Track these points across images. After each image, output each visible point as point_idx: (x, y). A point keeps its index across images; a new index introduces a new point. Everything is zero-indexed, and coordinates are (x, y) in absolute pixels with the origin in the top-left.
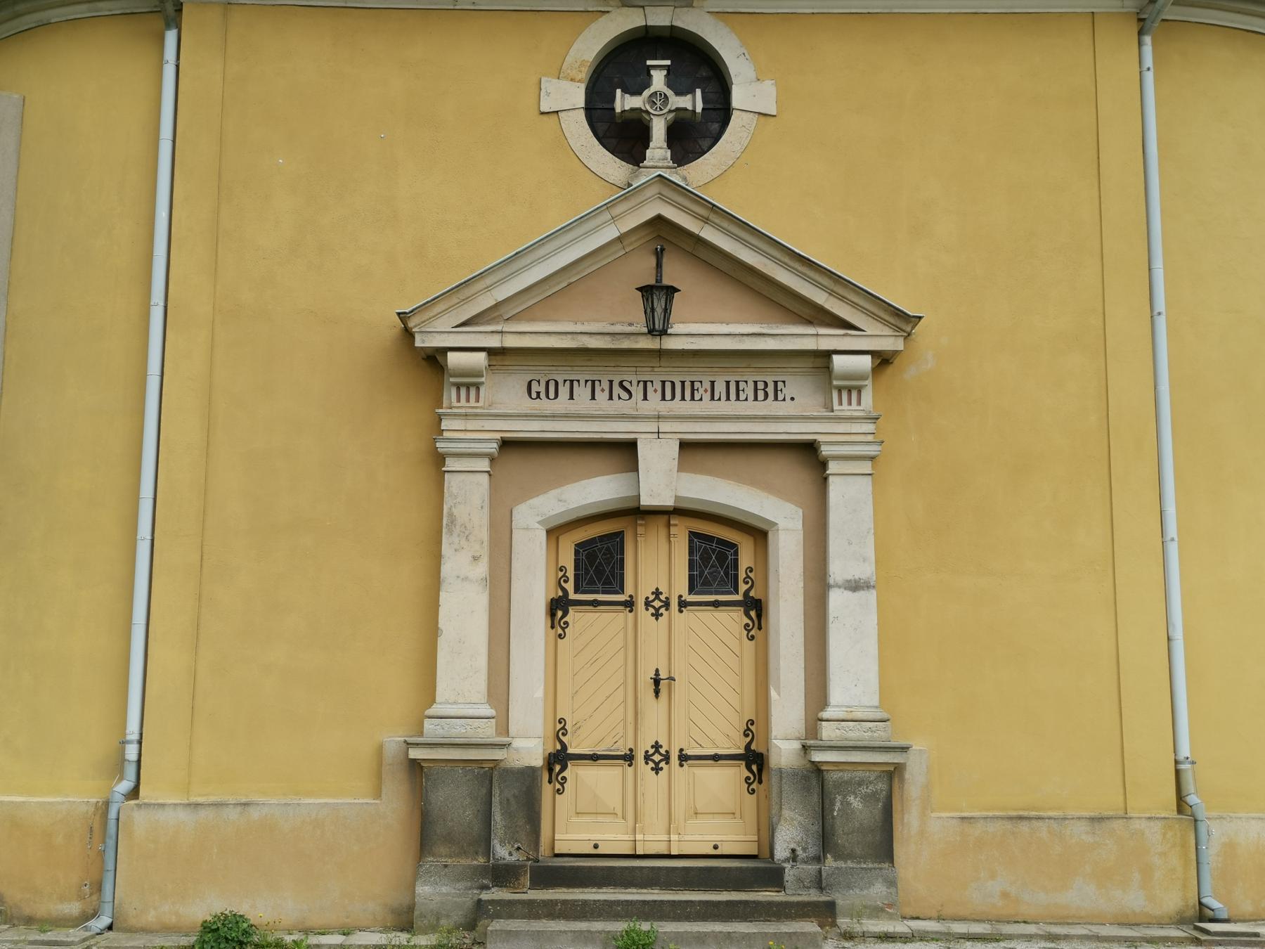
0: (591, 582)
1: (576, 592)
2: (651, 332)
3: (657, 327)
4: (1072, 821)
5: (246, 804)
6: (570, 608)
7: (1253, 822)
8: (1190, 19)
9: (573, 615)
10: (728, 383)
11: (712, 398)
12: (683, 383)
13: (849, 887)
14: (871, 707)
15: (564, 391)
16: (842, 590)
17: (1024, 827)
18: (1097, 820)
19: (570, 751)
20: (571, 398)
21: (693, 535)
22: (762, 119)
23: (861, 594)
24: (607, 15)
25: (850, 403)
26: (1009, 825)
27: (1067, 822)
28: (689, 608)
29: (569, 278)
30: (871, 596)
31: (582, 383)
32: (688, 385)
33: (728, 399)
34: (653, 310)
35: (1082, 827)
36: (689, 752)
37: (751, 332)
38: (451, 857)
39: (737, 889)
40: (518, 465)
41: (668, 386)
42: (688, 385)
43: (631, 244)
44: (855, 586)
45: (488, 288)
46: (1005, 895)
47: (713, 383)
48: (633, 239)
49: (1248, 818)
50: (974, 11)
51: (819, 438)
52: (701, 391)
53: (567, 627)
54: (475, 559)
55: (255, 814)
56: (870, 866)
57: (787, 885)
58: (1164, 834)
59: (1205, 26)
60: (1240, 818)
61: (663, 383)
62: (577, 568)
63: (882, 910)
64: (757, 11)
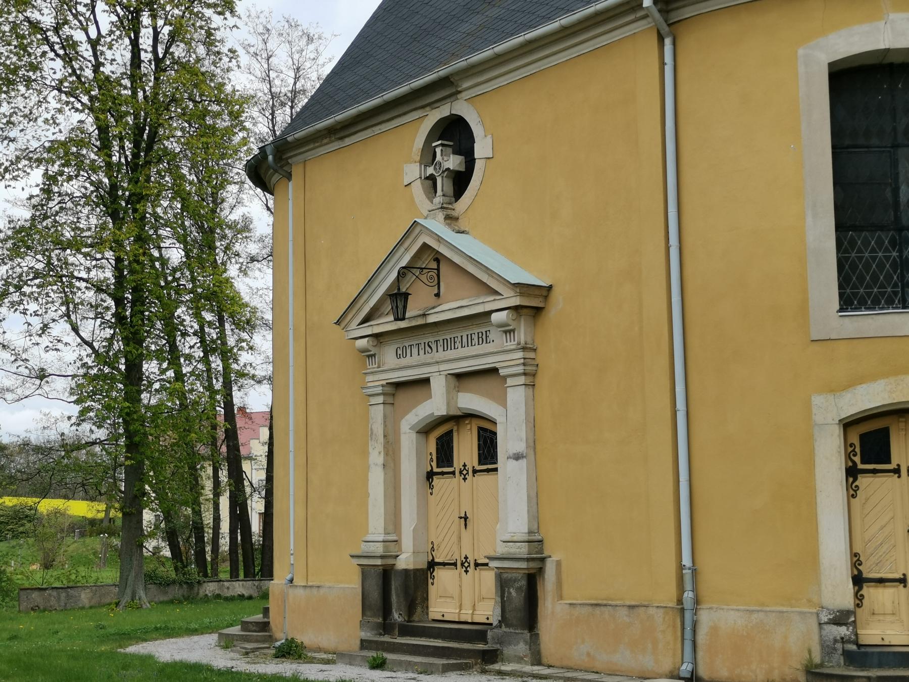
0: (443, 461)
1: (438, 467)
2: (397, 319)
3: (400, 317)
4: (620, 608)
5: (318, 587)
6: (434, 477)
7: (732, 613)
8: (702, 12)
9: (436, 481)
10: (467, 335)
11: (462, 347)
12: (451, 338)
13: (510, 644)
14: (523, 533)
15: (415, 351)
16: (512, 460)
17: (598, 611)
18: (631, 607)
19: (437, 560)
20: (411, 356)
21: (480, 429)
22: (488, 161)
23: (520, 461)
24: (427, 118)
25: (511, 341)
26: (590, 609)
27: (617, 608)
28: (478, 474)
29: (406, 285)
30: (523, 462)
31: (433, 342)
32: (452, 339)
33: (468, 346)
34: (397, 307)
35: (624, 612)
36: (479, 562)
37: (457, 306)
38: (371, 617)
39: (469, 642)
40: (403, 397)
41: (445, 340)
42: (452, 339)
43: (426, 260)
44: (517, 457)
45: (367, 301)
46: (588, 654)
47: (462, 336)
48: (426, 256)
49: (728, 609)
50: (577, 54)
51: (497, 365)
52: (458, 342)
53: (858, 490)
54: (380, 453)
55: (322, 591)
56: (520, 631)
57: (489, 641)
58: (664, 618)
59: (733, 7)
60: (723, 609)
61: (443, 340)
62: (437, 453)
63: (522, 658)
64: (485, 91)
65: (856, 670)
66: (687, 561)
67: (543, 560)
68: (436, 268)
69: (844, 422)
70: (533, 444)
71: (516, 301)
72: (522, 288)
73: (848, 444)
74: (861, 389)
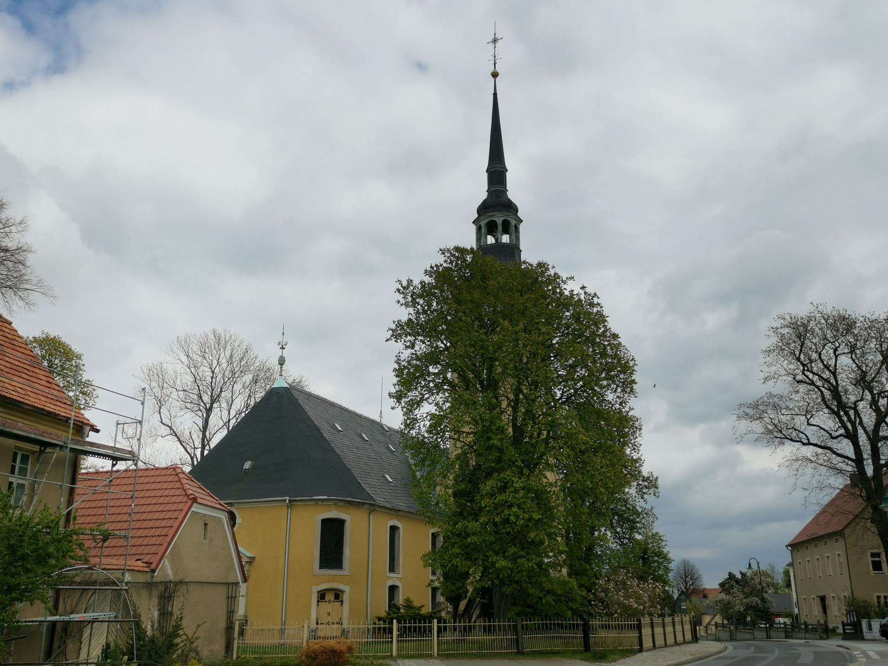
30: (244, 597)
44: (243, 596)
65: (399, 596)
66: (283, 620)
67: (247, 620)
68: (686, 641)
69: (871, 569)
70: (247, 593)
71: (248, 560)
72: (250, 558)
73: (318, 596)
74: (322, 585)
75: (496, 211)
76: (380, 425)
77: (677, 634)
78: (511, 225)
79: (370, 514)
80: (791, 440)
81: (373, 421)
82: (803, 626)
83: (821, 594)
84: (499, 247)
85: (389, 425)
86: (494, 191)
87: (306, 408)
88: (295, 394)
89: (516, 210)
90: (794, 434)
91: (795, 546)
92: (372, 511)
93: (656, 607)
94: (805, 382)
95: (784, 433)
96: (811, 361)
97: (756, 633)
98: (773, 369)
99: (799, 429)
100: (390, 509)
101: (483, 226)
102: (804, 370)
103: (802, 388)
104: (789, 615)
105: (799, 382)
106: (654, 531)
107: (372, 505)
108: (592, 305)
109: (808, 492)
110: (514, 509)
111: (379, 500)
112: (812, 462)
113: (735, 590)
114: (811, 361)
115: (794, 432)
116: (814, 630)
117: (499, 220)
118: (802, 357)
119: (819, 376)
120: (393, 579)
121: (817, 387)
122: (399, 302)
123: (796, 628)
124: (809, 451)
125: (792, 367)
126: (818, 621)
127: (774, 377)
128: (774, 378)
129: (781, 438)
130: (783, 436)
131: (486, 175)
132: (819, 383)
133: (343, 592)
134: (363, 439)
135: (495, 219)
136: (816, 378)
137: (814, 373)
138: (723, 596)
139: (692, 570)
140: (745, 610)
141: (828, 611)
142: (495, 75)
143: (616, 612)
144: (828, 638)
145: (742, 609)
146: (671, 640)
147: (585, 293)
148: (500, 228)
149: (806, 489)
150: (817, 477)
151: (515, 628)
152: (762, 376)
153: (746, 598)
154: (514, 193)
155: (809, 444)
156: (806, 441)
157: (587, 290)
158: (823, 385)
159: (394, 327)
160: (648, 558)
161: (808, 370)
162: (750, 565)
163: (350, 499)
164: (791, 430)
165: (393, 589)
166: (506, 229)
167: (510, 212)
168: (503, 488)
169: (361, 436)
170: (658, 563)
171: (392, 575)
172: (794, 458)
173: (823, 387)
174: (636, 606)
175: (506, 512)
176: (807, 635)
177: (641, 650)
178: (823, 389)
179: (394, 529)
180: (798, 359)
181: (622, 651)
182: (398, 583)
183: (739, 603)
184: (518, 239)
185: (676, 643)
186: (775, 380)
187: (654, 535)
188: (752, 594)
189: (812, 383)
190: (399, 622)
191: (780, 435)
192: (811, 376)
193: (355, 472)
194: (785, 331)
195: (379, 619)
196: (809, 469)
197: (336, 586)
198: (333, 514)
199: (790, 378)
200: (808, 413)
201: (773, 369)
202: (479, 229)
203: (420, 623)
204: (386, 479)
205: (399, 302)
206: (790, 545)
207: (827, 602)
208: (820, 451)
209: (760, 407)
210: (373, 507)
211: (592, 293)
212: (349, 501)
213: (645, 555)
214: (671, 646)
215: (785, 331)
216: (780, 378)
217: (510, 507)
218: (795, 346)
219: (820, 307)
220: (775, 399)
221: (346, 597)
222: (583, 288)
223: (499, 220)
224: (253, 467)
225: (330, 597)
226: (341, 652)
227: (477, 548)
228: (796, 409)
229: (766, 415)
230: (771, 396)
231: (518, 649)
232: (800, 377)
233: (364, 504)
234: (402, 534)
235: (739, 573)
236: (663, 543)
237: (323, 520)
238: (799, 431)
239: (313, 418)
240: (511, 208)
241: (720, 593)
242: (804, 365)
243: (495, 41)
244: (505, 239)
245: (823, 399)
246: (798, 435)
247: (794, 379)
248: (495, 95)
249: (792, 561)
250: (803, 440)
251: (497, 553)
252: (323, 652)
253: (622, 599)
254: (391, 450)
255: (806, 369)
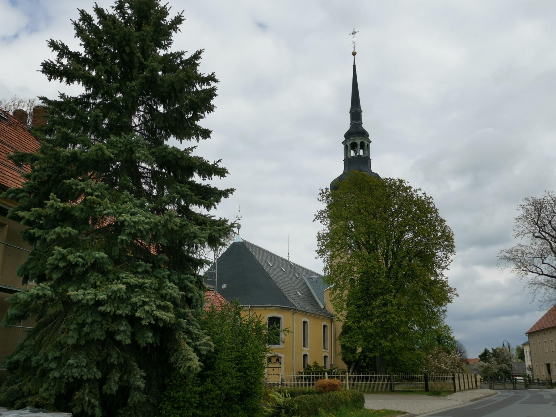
75: (356, 136)
76: (287, 262)
77: (461, 384)
78: (365, 146)
79: (293, 315)
80: (532, 272)
81: (285, 260)
82: (536, 381)
83: (547, 362)
84: (358, 158)
85: (293, 262)
86: (354, 124)
87: (253, 253)
88: (247, 245)
89: (368, 136)
90: (534, 268)
91: (530, 334)
92: (295, 313)
93: (456, 369)
94: (542, 238)
95: (528, 268)
96: (544, 225)
97: (507, 385)
98: (521, 229)
99: (537, 265)
100: (303, 312)
101: (348, 145)
102: (540, 230)
103: (540, 242)
104: (524, 376)
105: (537, 237)
106: (445, 324)
107: (294, 309)
108: (429, 203)
109: (542, 303)
110: (393, 315)
111: (298, 306)
112: (544, 285)
113: (492, 360)
114: (544, 225)
115: (534, 267)
116: (544, 383)
117: (358, 142)
118: (539, 223)
119: (549, 234)
120: (305, 351)
121: (548, 240)
122: (318, 199)
123: (529, 383)
124: (542, 278)
125: (532, 228)
126: (546, 378)
127: (523, 234)
128: (521, 235)
129: (526, 271)
130: (527, 269)
131: (349, 114)
132: (548, 238)
133: (281, 357)
134: (283, 270)
135: (356, 141)
136: (547, 235)
137: (546, 233)
138: (482, 363)
139: (460, 347)
140: (499, 372)
141: (551, 372)
142: (354, 54)
143: (433, 371)
144: (552, 388)
145: (496, 371)
146: (467, 387)
147: (425, 196)
148: (359, 147)
149: (541, 301)
150: (547, 294)
151: (390, 378)
152: (514, 233)
153: (499, 364)
154: (366, 124)
155: (543, 274)
156: (540, 273)
157: (426, 195)
158: (551, 239)
159: (317, 214)
160: (441, 340)
161: (542, 231)
162: (503, 345)
163: (284, 306)
164: (532, 266)
165: (305, 356)
166: (362, 146)
167: (364, 137)
168: (385, 305)
169: (281, 269)
170: (447, 343)
171: (304, 349)
172: (534, 282)
173: (551, 240)
174: (445, 368)
175: (388, 316)
176: (539, 386)
177: (455, 391)
178: (551, 242)
179: (305, 323)
180: (537, 224)
181: (445, 391)
182: (307, 353)
183: (494, 367)
184: (369, 153)
185: (469, 389)
186: (522, 236)
187: (446, 327)
188: (502, 362)
189: (545, 238)
190: (328, 374)
191: (525, 269)
192: (544, 234)
193: (283, 290)
194: (529, 207)
195: (299, 373)
196: (543, 290)
197: (280, 355)
198: (275, 314)
199: (531, 235)
200: (542, 257)
201: (521, 229)
202: (346, 147)
203: (313, 374)
204: (298, 294)
205: (318, 199)
206: (528, 333)
207: (551, 367)
208: (549, 278)
209: (513, 253)
210: (295, 311)
211: (429, 197)
212: (283, 307)
213: (439, 338)
214: (467, 390)
215: (529, 207)
216: (525, 235)
217: (391, 313)
218: (535, 215)
219: (551, 194)
220: (523, 248)
221: (282, 361)
222: (424, 193)
223: (358, 142)
224: (227, 288)
225: (273, 360)
226: (337, 385)
227: (371, 335)
228: (535, 253)
229: (517, 257)
230: (521, 246)
231: (391, 389)
232: (537, 234)
233: (290, 309)
234: (309, 325)
235: (491, 349)
236: (451, 331)
237: (269, 318)
238: (537, 267)
239: (258, 259)
240: (364, 134)
241: (480, 361)
242: (540, 228)
243: (354, 33)
244: (361, 152)
245: (552, 248)
246: (536, 269)
247: (534, 235)
248: (354, 66)
249: (529, 341)
250: (539, 272)
251: (381, 338)
252: (329, 385)
253: (436, 364)
254: (296, 277)
255: (541, 230)
